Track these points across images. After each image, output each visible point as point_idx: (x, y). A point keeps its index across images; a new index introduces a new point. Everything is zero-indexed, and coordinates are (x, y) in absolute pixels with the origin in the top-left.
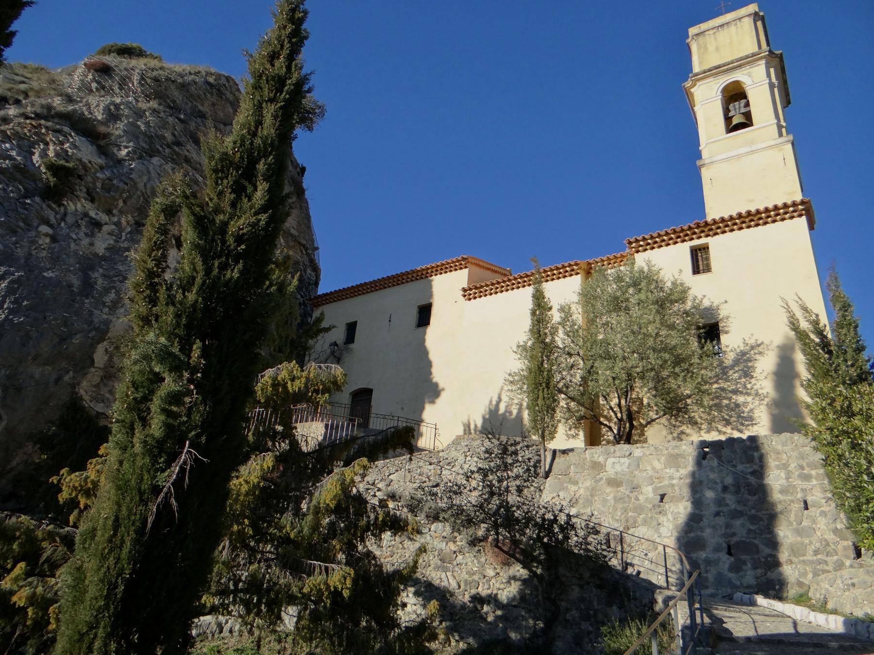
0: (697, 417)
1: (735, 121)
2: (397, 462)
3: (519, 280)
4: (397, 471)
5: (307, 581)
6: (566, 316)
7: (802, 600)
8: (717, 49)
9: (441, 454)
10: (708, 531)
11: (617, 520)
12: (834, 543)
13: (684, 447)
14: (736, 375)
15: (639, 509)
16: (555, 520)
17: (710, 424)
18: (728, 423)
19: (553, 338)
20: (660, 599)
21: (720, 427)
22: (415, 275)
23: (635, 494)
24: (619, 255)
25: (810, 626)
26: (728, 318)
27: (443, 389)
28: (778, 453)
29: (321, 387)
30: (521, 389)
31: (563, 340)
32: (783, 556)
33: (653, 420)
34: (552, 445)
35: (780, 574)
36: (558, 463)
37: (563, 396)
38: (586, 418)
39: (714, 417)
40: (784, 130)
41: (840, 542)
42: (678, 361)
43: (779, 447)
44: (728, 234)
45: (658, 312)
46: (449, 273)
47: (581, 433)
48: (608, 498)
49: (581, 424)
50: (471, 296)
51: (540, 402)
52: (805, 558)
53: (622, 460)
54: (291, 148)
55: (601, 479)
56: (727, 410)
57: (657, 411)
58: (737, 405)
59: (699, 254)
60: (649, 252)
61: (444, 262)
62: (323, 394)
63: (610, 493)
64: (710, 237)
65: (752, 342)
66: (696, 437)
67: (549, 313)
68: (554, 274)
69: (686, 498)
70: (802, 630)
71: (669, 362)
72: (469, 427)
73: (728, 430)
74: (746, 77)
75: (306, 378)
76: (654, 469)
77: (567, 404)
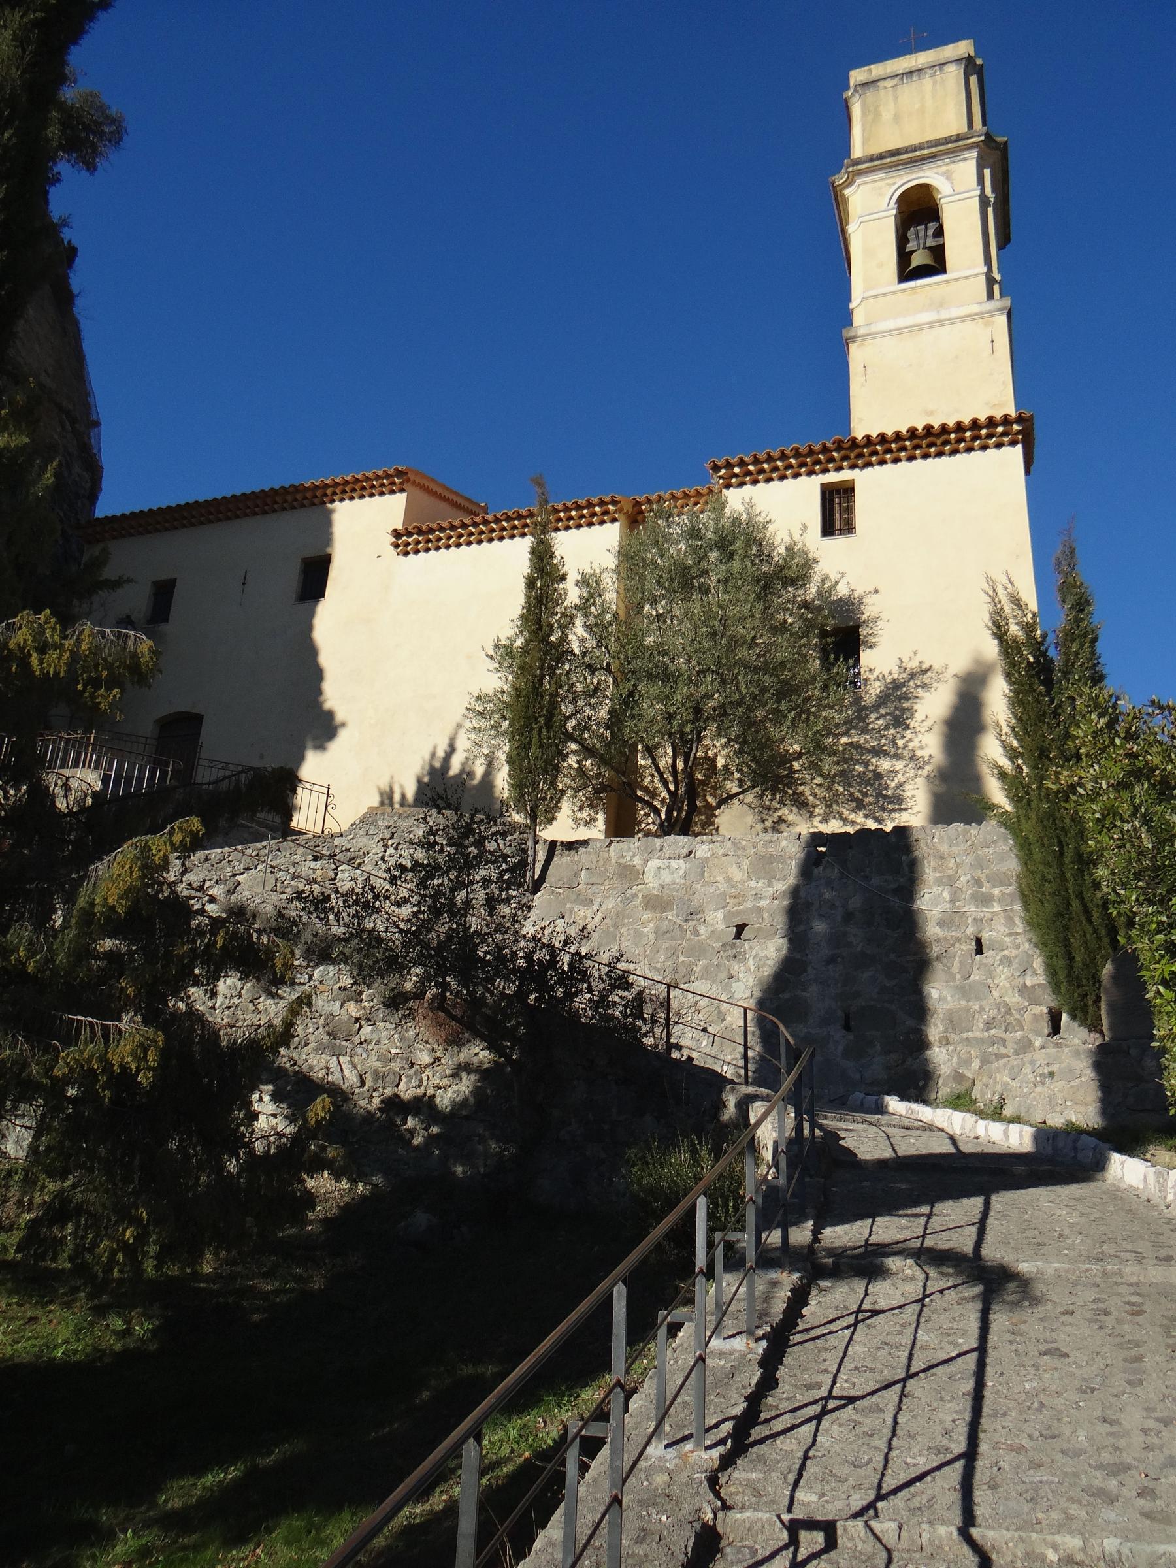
0: (807, 793)
1: (917, 260)
2: (248, 852)
3: (505, 524)
4: (248, 869)
5: (63, 1054)
6: (591, 595)
7: (961, 1101)
8: (897, 118)
9: (337, 841)
10: (814, 989)
11: (658, 970)
12: (1019, 1010)
13: (784, 843)
14: (880, 722)
15: (698, 951)
16: (553, 963)
17: (829, 806)
18: (859, 805)
19: (563, 633)
20: (731, 1102)
21: (846, 813)
22: (299, 496)
23: (692, 923)
24: (692, 492)
25: (978, 1143)
26: (876, 620)
27: (343, 725)
28: (942, 858)
29: (105, 673)
30: (495, 727)
31: (582, 641)
32: (934, 1032)
33: (731, 797)
34: (549, 833)
35: (926, 1062)
36: (558, 866)
37: (573, 746)
38: (612, 789)
39: (837, 794)
40: (996, 287)
41: (1029, 1008)
42: (786, 691)
43: (945, 848)
44: (889, 467)
45: (759, 598)
46: (367, 499)
47: (601, 817)
48: (646, 930)
49: (601, 799)
50: (409, 548)
51: (534, 751)
52: (971, 1034)
53: (674, 864)
54: (47, 202)
55: (635, 896)
56: (860, 784)
57: (740, 780)
58: (878, 776)
59: (837, 501)
60: (748, 488)
61: (359, 476)
62: (109, 689)
63: (648, 922)
64: (857, 470)
65: (913, 665)
66: (805, 828)
67: (561, 586)
68: (571, 518)
69: (781, 932)
70: (967, 1148)
71: (771, 691)
72: (391, 798)
73: (860, 818)
74: (942, 179)
75: (72, 652)
76: (729, 880)
77: (579, 762)
